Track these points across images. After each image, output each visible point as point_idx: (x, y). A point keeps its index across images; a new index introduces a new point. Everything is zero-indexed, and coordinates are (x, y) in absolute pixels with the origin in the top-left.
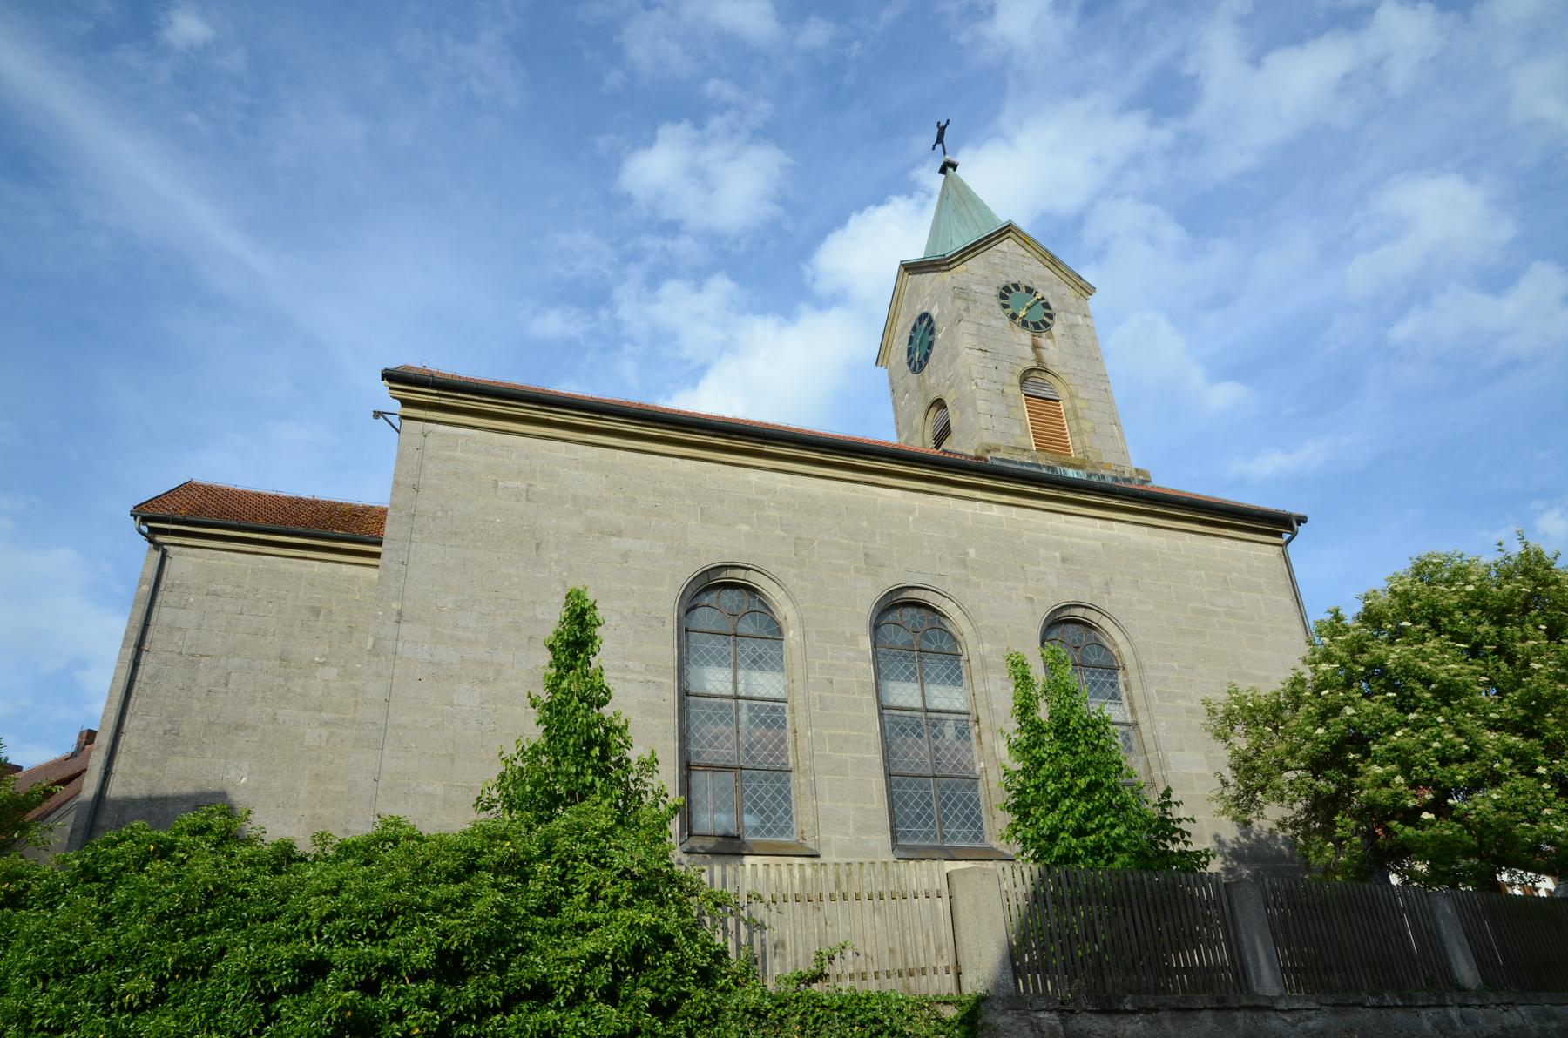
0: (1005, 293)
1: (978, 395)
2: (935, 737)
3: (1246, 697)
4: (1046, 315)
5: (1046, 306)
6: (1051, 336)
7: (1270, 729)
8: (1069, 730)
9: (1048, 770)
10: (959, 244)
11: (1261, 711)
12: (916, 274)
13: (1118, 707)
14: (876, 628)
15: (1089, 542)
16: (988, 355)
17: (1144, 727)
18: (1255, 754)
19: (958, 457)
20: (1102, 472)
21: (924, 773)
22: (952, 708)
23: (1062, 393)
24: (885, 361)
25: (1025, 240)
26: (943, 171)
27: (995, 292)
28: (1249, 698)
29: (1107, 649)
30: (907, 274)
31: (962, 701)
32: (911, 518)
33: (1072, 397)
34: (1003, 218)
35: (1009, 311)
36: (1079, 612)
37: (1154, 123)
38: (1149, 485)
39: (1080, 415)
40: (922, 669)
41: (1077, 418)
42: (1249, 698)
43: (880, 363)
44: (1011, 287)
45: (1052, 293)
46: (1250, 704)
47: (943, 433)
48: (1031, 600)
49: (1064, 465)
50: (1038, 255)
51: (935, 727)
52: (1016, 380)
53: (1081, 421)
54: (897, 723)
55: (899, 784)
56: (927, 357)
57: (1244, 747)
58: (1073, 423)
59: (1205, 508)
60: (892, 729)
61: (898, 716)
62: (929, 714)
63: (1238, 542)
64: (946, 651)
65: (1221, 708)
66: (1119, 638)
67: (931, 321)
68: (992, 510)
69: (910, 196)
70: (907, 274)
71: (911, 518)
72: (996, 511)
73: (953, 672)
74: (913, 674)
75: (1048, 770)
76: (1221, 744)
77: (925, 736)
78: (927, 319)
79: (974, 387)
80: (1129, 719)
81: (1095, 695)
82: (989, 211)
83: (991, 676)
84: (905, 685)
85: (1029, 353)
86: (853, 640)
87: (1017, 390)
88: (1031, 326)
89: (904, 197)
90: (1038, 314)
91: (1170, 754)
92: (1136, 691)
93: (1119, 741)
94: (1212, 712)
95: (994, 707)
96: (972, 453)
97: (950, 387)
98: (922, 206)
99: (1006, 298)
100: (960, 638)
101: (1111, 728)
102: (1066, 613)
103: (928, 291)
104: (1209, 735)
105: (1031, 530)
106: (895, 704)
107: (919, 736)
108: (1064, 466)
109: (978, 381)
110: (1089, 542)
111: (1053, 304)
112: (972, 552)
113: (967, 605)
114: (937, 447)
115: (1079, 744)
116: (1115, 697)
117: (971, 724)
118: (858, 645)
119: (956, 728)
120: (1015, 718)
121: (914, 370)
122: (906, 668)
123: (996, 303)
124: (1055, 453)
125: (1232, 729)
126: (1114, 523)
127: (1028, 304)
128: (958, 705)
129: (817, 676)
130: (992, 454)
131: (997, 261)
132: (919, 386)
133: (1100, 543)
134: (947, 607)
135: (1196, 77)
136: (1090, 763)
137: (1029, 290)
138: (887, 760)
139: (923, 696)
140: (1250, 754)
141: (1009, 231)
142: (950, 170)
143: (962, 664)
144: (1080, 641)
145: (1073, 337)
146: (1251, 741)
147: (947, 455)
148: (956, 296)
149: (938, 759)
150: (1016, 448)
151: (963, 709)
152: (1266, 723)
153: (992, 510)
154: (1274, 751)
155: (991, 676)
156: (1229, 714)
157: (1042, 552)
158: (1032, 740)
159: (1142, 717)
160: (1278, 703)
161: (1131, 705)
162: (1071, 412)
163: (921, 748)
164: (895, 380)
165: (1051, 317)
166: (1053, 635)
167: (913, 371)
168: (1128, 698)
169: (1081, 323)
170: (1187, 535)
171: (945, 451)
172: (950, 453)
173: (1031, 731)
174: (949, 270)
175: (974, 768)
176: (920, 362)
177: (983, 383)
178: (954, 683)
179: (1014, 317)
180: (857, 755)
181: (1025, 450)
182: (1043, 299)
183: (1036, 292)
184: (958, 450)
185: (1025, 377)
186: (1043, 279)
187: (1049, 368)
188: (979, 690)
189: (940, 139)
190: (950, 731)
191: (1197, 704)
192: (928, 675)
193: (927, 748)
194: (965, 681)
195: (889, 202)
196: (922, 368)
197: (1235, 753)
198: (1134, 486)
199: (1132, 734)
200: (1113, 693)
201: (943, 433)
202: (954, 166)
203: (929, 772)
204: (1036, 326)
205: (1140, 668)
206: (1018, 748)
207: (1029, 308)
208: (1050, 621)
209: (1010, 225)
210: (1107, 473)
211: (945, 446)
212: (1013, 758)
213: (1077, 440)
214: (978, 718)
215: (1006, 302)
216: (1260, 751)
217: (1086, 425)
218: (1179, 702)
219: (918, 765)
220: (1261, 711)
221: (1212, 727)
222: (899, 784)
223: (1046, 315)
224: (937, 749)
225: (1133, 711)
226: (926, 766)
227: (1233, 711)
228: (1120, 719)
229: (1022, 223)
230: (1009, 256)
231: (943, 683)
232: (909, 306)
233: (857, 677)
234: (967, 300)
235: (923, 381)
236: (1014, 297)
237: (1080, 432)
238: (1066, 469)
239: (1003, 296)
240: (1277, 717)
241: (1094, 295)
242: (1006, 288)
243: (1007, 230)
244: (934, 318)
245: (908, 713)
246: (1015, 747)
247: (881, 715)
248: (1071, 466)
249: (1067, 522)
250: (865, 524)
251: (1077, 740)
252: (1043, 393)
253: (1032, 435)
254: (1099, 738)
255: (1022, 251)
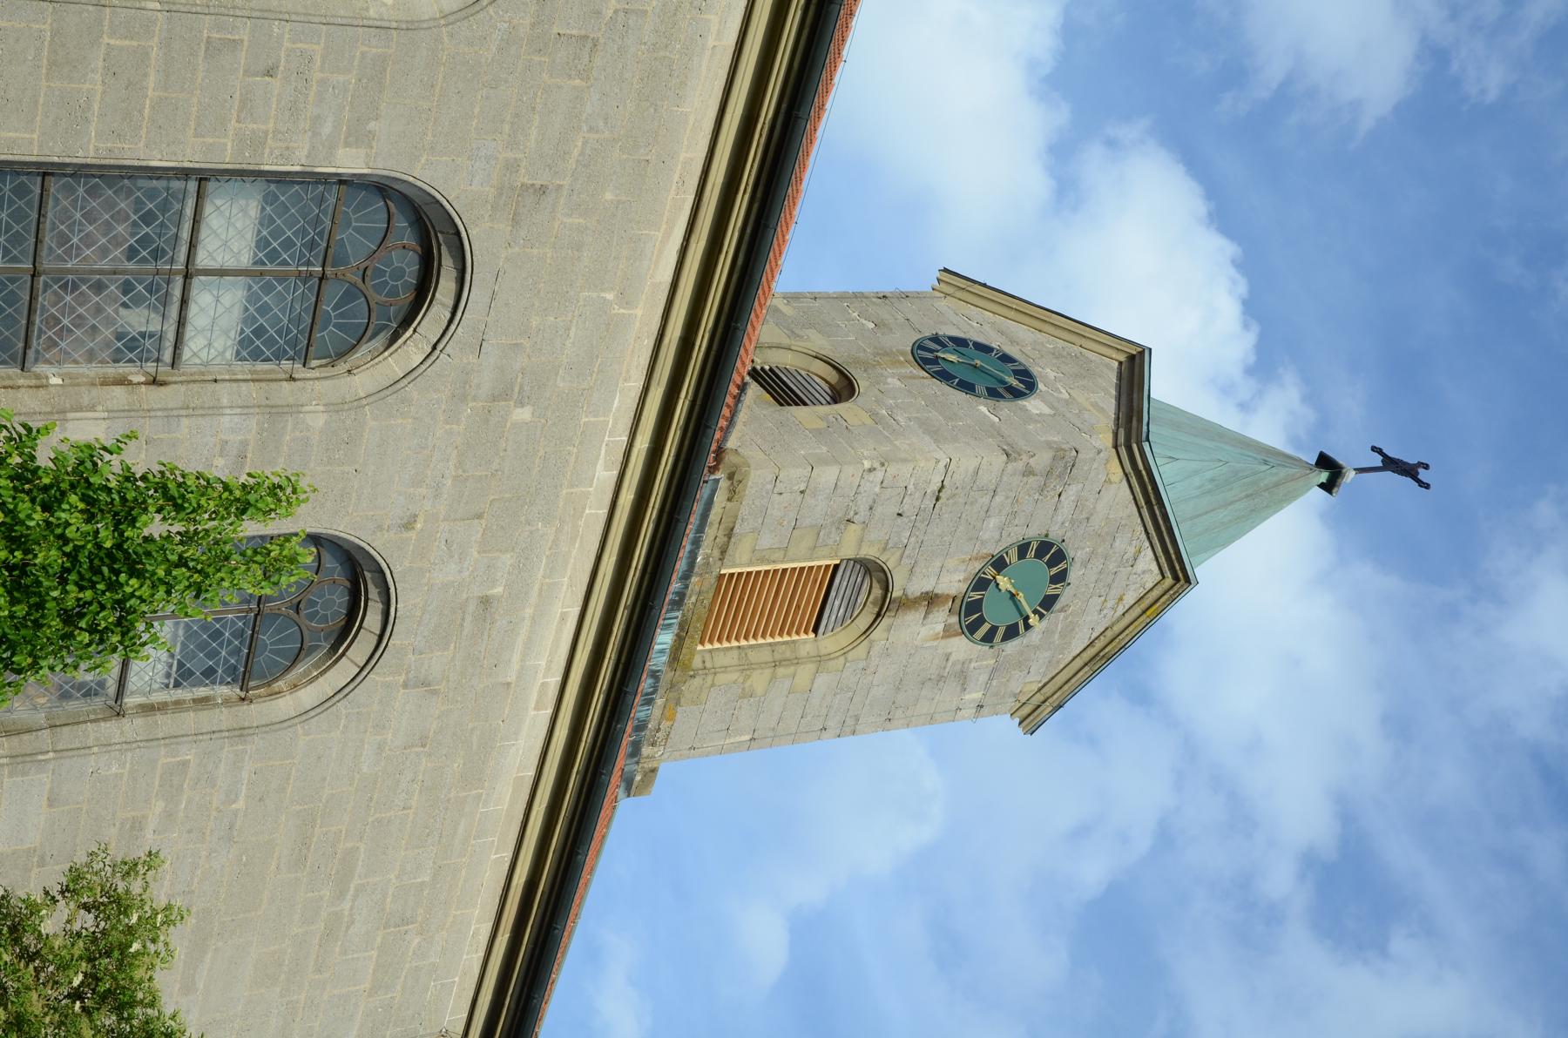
0: (1051, 554)
1: (849, 470)
2: (127, 288)
3: (154, 941)
4: (994, 630)
5: (1012, 633)
6: (948, 633)
7: (76, 982)
8: (117, 573)
9: (29, 517)
10: (1167, 473)
11: (120, 968)
12: (1120, 377)
13: (160, 679)
14: (382, 189)
15: (516, 658)
16: (929, 503)
17: (111, 729)
18: (26, 948)
19: (726, 412)
20: (659, 702)
21: (44, 253)
22: (189, 332)
23: (830, 641)
24: (950, 290)
25: (1152, 608)
26: (1324, 462)
27: (1054, 536)
28: (151, 947)
29: (288, 669)
30: (1122, 358)
31: (203, 355)
32: (610, 296)
33: (820, 660)
34: (1203, 571)
35: (1013, 557)
36: (373, 620)
37: (1309, 862)
38: (621, 792)
39: (781, 671)
40: (282, 278)
41: (776, 664)
42: (151, 947)
43: (946, 277)
44: (1062, 566)
45: (1037, 648)
46: (136, 947)
47: (781, 389)
48: (408, 525)
49: (684, 627)
50: (1117, 629)
51: (149, 289)
52: (869, 552)
53: (768, 672)
54: (165, 207)
55: (21, 191)
56: (944, 376)
57: (47, 927)
58: (765, 656)
59: (545, 942)
60: (152, 194)
61: (181, 213)
62: (179, 280)
63: (481, 954)
64: (317, 335)
65: (136, 887)
66: (308, 696)
67: (1017, 394)
68: (607, 468)
69: (1250, 371)
70: (1122, 358)
71: (610, 296)
72: (605, 475)
73: (270, 342)
74: (273, 256)
75: (29, 517)
76: (55, 878)
77: (131, 266)
78: (1021, 386)
79: (867, 464)
80: (130, 701)
81: (190, 634)
82: (1225, 544)
83: (252, 423)
84: (250, 237)
85: (918, 587)
86: (358, 136)
87: (848, 552)
88: (976, 596)
89: (1252, 359)
90: (997, 613)
91: (46, 778)
92: (190, 720)
93: (84, 676)
94: (130, 869)
95: (185, 421)
96: (731, 444)
97: (874, 415)
98: (1226, 390)
99: (1039, 554)
100: (342, 367)
101: (115, 662)
102: (374, 593)
103: (1080, 397)
104: (81, 859)
105: (556, 542)
106: (208, 209)
107: (132, 253)
108: (681, 626)
109: (879, 475)
110: (516, 658)
111: (1012, 646)
112: (523, 414)
113: (412, 391)
114: (754, 373)
115: (82, 589)
116: (182, 675)
117: (150, 367)
118: (347, 144)
119: (143, 335)
120: (156, 468)
121: (921, 347)
122: (288, 244)
123: (1033, 533)
124: (711, 611)
125: (87, 908)
126: (550, 711)
127: (1021, 597)
128: (194, 345)
129: (287, 44)
130: (724, 484)
131: (1119, 544)
132: (886, 354)
133: (512, 678)
134: (412, 348)
135: (1383, 952)
136: (40, 606)
137: (1048, 602)
138: (80, 172)
139: (222, 273)
140: (29, 940)
141: (1176, 579)
142: (1324, 476)
143: (286, 365)
144: (311, 617)
145: (941, 678)
146: (57, 943)
147: (733, 390)
148: (1059, 454)
149: (75, 287)
150: (730, 534)
151: (186, 353)
152: (93, 978)
153: (607, 468)
154: (28, 988)
155: (252, 423)
156: (119, 904)
157: (507, 559)
158: (103, 496)
159: (132, 727)
160: (132, 1004)
161: (162, 707)
162: (788, 655)
163: (104, 252)
164: (907, 303)
165: (988, 638)
166: (329, 562)
167: (919, 346)
168: (178, 703)
169: (968, 697)
170: (508, 855)
171: (743, 388)
172: (738, 399)
173: (124, 499)
174: (1116, 447)
175: (49, 362)
176: (935, 361)
177: (872, 485)
178: (244, 342)
179: (1000, 564)
180: (96, 107)
181: (723, 552)
182: (1028, 627)
183: (1041, 616)
184: (742, 416)
185: (873, 571)
186: (1069, 631)
187: (886, 622)
188: (225, 393)
189: (1391, 464)
190: (138, 320)
191: (149, 840)
192: (268, 289)
193: (104, 264)
194: (247, 365)
195: (1246, 326)
196: (923, 363)
197: (34, 909)
198: (621, 761)
199: (98, 702)
200: (191, 673)
201: (781, 389)
202: (1328, 487)
203: (46, 263)
204: (975, 607)
205: (240, 733)
206: (89, 465)
207: (1013, 596)
208: (358, 557)
209: (1188, 581)
210: (656, 710)
211: (754, 389)
212: (64, 448)
213: (732, 659)
214: (163, 384)
215: (1031, 553)
216: (31, 959)
217: (759, 680)
218: (159, 806)
219: (63, 240)
220: (120, 966)
221: (97, 867)
222: (21, 191)
223: (994, 630)
224: (99, 287)
225: (148, 709)
226: (60, 258)
227: (126, 911)
228: (133, 681)
229: (1186, 610)
230: (1125, 571)
231: (248, 319)
232: (1056, 355)
233: (276, 131)
234: (1049, 474)
235: (897, 363)
236: (1039, 569)
237: (747, 668)
238: (675, 629)
239: (1044, 547)
240: (104, 997)
241: (1020, 731)
242: (1060, 557)
243: (1178, 575)
244: (1021, 402)
245: (185, 234)
246: (89, 458)
247: (185, 174)
248: (680, 641)
249: (563, 618)
250: (609, 196)
251: (93, 586)
252: (835, 602)
253: (754, 569)
254: (92, 629)
255: (1130, 599)
